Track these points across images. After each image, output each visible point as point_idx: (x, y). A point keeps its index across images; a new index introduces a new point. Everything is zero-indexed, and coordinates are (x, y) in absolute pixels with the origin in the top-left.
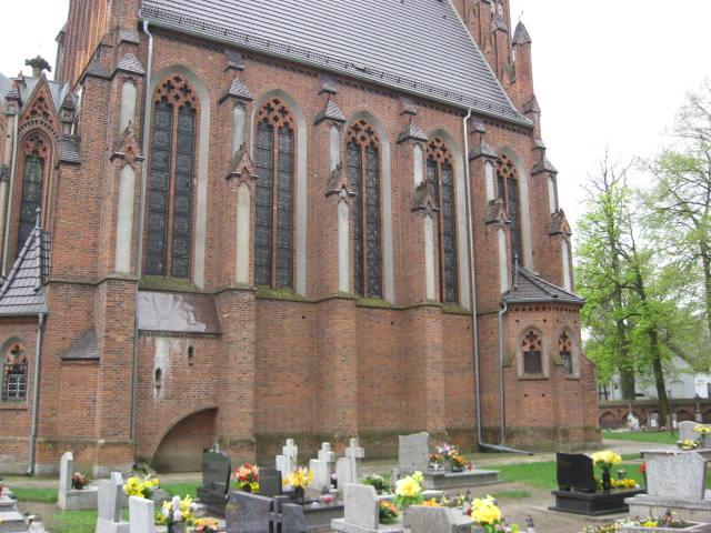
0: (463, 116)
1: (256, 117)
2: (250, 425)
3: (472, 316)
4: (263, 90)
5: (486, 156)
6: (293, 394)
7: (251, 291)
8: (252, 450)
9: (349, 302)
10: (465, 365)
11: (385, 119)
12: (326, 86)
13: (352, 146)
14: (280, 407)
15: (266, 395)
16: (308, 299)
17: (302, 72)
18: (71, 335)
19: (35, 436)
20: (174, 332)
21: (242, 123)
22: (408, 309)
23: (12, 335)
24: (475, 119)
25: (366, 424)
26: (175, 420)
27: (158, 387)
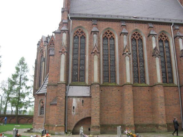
0: (171, 25)
1: (102, 36)
2: (99, 122)
3: (178, 87)
4: (104, 28)
5: (179, 36)
6: (116, 113)
7: (98, 84)
8: (99, 129)
9: (130, 85)
10: (176, 103)
11: (143, 30)
12: (122, 24)
13: (133, 40)
14: (112, 116)
15: (107, 113)
16: (120, 85)
17: (162, 25)
18: (52, 98)
19: (45, 124)
20: (78, 96)
21: (126, 41)
22: (152, 86)
24: (175, 25)
25: (140, 122)
26: (78, 120)
27: (74, 111)
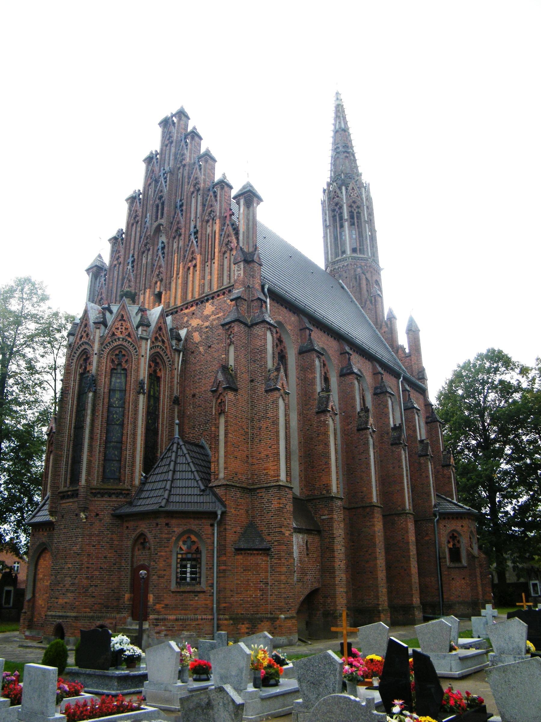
23: (186, 528)
